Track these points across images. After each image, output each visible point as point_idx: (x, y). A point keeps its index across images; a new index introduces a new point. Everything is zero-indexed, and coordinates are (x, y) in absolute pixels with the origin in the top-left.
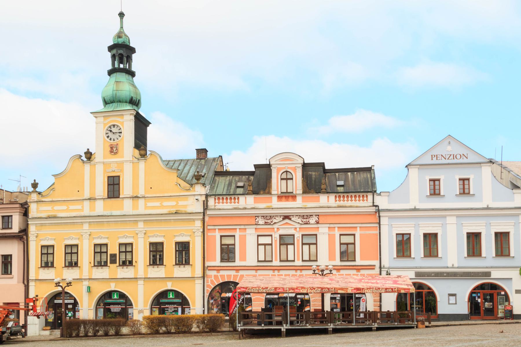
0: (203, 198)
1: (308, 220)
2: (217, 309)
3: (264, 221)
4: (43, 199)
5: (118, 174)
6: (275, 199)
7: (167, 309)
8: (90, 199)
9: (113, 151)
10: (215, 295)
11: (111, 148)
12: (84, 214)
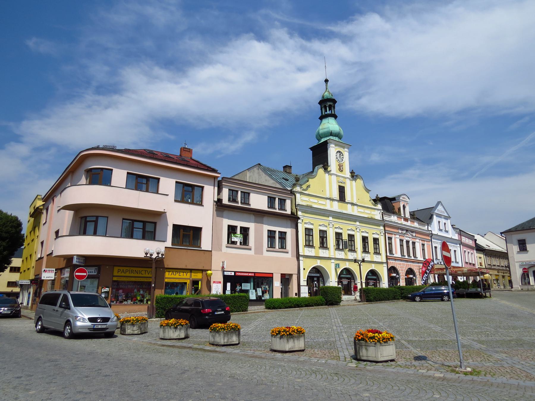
6: (403, 220)
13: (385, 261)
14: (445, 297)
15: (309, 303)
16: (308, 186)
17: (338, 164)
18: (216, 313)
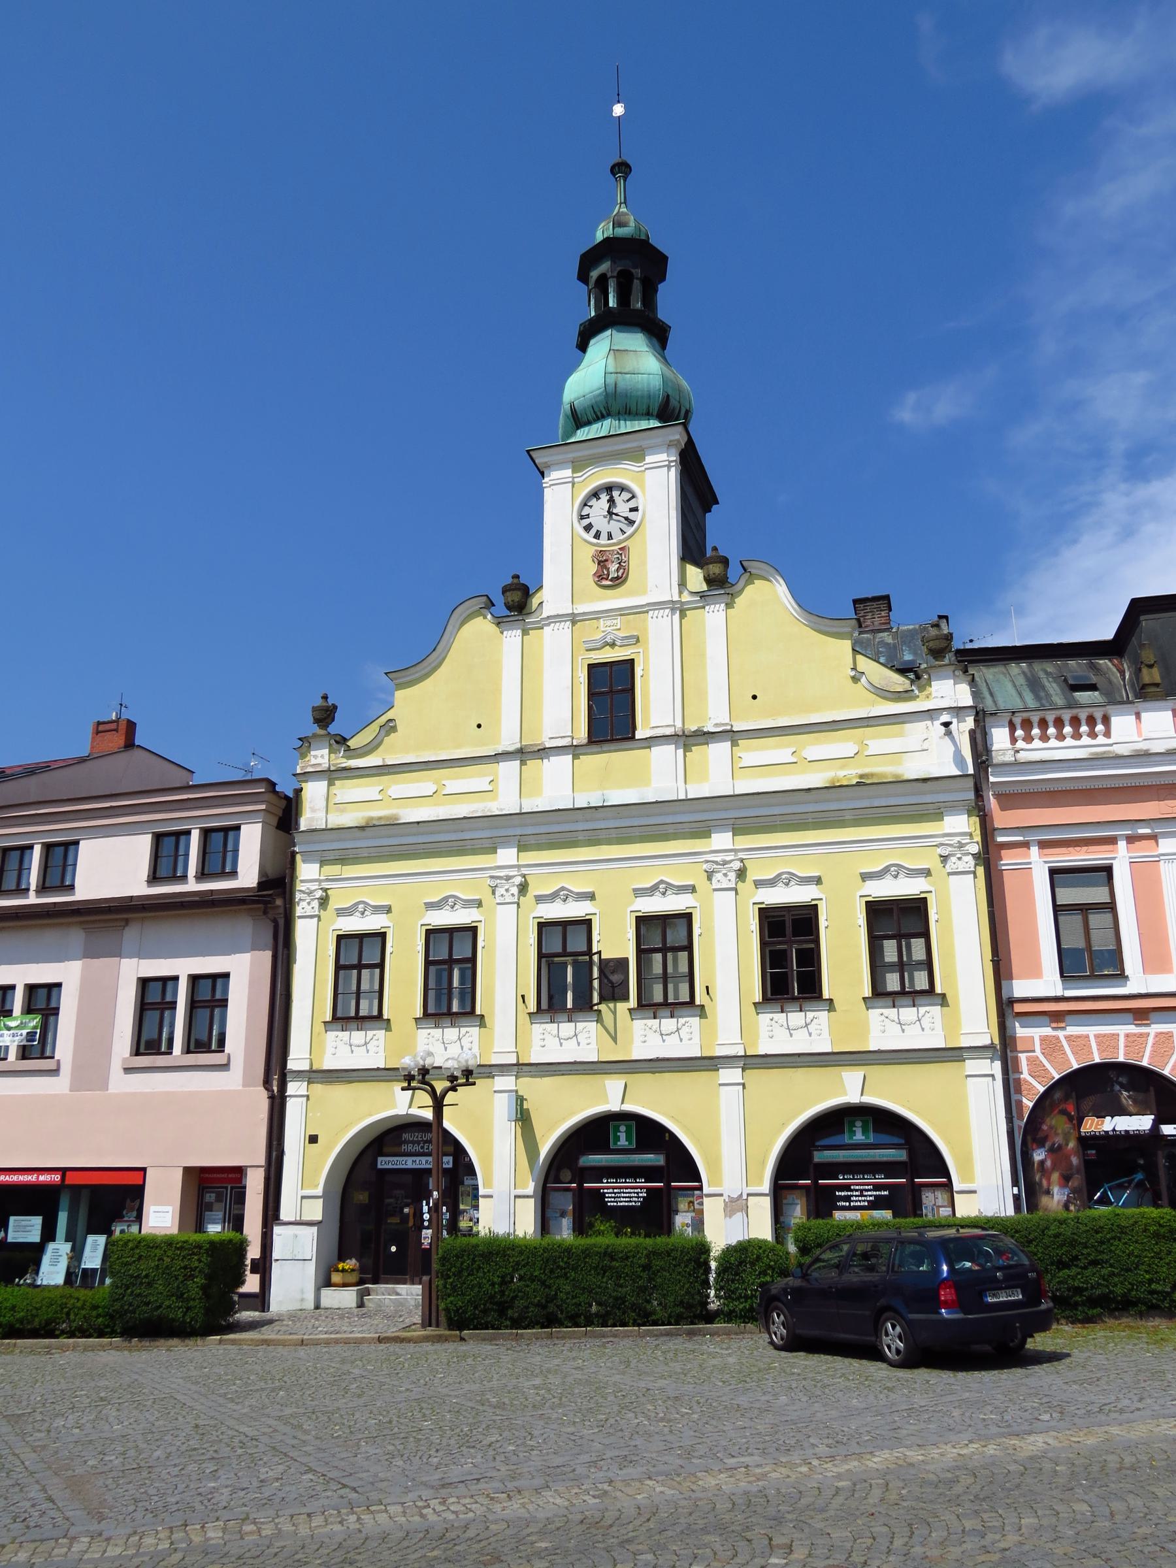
2: (1066, 1191)
12: (501, 810)
14: (898, 1329)
15: (21, 1321)
16: (390, 727)
18: (990, 1300)
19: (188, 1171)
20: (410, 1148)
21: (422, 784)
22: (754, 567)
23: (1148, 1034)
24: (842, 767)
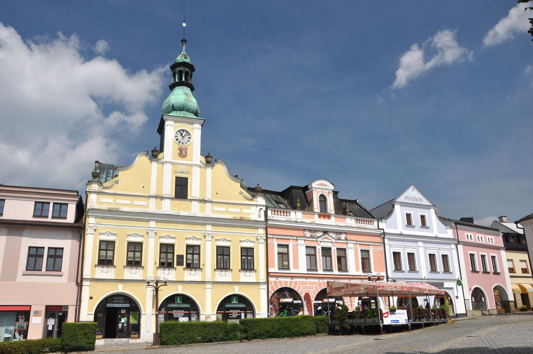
0: (264, 209)
1: (340, 237)
2: (276, 314)
3: (310, 234)
4: (105, 191)
5: (187, 176)
6: (316, 216)
7: (231, 315)
8: (156, 197)
9: (182, 154)
10: (274, 300)
11: (180, 150)
12: (150, 211)
13: (265, 281)
17: (178, 146)
19: (46, 305)
20: (116, 301)
21: (127, 201)
22: (219, 161)
23: (293, 282)
24: (237, 215)
